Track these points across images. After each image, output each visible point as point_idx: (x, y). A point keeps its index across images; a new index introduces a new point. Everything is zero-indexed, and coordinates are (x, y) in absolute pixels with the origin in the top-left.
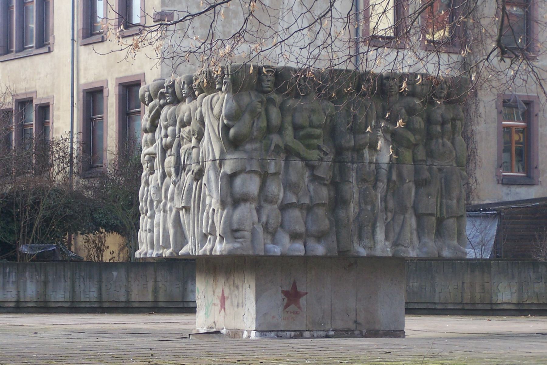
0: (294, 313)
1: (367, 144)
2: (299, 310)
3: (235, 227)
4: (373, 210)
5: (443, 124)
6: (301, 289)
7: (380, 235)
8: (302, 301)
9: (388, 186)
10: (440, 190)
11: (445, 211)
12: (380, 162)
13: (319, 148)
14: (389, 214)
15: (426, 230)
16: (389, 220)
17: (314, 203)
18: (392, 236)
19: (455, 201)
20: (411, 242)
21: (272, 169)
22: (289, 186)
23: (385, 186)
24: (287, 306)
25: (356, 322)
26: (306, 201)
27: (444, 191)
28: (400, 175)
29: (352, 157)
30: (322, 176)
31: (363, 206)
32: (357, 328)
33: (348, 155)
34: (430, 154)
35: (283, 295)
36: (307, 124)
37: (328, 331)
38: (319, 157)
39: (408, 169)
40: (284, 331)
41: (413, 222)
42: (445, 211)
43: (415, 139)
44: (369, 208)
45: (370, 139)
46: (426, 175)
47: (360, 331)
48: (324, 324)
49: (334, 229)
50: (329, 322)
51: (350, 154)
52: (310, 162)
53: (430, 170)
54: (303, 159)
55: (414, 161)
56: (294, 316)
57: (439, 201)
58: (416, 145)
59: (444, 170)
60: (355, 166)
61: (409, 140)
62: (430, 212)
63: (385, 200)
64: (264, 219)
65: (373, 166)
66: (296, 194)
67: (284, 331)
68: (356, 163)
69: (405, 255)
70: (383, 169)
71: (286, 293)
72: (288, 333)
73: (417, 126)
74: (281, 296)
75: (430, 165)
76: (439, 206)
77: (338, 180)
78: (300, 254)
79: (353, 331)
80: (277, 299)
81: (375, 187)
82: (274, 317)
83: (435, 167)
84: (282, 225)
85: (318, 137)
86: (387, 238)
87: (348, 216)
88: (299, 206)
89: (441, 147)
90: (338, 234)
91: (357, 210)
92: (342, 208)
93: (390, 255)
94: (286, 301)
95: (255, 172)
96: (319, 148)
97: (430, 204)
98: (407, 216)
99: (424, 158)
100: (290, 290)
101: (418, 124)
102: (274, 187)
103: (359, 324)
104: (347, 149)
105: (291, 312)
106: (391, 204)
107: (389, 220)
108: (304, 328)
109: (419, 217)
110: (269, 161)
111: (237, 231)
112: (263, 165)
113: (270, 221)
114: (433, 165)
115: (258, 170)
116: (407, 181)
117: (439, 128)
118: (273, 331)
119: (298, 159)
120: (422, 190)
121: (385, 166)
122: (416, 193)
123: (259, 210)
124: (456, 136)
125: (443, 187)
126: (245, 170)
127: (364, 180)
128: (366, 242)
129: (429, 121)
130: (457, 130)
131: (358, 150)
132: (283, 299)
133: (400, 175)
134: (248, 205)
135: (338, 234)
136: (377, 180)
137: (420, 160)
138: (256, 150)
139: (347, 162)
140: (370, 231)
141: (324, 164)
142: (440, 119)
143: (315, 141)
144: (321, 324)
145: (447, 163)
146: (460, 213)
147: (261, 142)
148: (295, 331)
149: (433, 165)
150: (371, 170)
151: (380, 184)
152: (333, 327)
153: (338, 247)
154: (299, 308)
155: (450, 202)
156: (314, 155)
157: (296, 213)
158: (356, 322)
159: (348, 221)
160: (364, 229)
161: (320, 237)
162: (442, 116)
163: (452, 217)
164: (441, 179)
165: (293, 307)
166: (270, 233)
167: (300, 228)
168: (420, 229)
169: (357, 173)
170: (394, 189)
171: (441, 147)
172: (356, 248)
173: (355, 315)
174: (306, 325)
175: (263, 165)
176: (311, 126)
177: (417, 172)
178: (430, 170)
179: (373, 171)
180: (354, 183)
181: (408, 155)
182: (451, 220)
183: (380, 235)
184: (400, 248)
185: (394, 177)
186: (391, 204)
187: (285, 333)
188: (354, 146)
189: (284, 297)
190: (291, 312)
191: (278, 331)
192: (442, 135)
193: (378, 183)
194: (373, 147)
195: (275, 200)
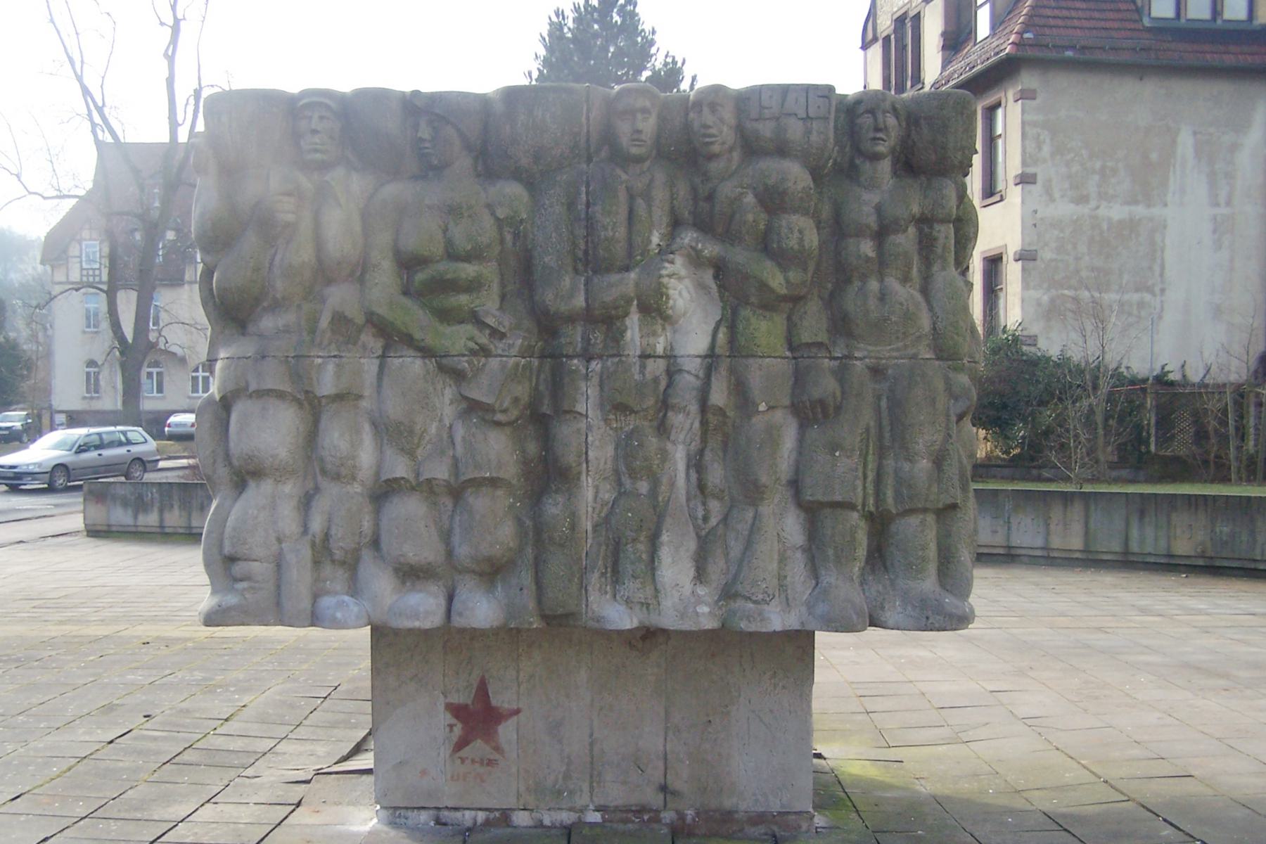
0: (482, 763)
1: (629, 302)
2: (497, 756)
3: (227, 550)
4: (654, 492)
5: (881, 234)
6: (501, 699)
7: (675, 569)
8: (506, 732)
9: (704, 423)
10: (873, 431)
11: (890, 493)
12: (676, 353)
13: (475, 319)
14: (714, 505)
15: (831, 552)
16: (713, 521)
17: (463, 478)
18: (717, 569)
19: (924, 464)
20: (782, 587)
21: (327, 384)
22: (392, 433)
23: (697, 425)
24: (461, 745)
25: (664, 788)
26: (440, 471)
27: (887, 435)
28: (740, 389)
29: (586, 340)
30: (484, 399)
31: (627, 482)
32: (669, 805)
33: (574, 336)
34: (841, 326)
35: (449, 716)
36: (438, 249)
37: (582, 810)
38: (471, 344)
39: (768, 369)
40: (456, 809)
41: (793, 527)
42: (890, 493)
43: (788, 281)
44: (644, 487)
45: (637, 285)
46: (826, 386)
47: (677, 812)
48: (571, 793)
49: (529, 550)
50: (586, 787)
51: (579, 329)
52: (444, 361)
53: (841, 374)
54: (426, 352)
55: (791, 348)
56: (481, 770)
57: (871, 466)
58: (796, 300)
59: (890, 371)
60: (596, 366)
61: (763, 286)
62: (838, 498)
63: (697, 464)
64: (317, 525)
65: (656, 367)
66: (411, 454)
67: (456, 809)
68: (600, 357)
69: (753, 628)
70: (689, 372)
71: (457, 711)
72: (467, 813)
73: (793, 243)
74: (445, 718)
75: (845, 357)
76: (871, 476)
77: (546, 408)
78: (417, 624)
79: (657, 811)
80: (439, 726)
81: (663, 429)
82: (424, 773)
83: (858, 363)
84: (376, 543)
85: (473, 286)
86: (701, 575)
87: (573, 515)
88: (427, 488)
89: (872, 303)
90: (538, 566)
91: (608, 495)
92: (556, 492)
93: (709, 624)
94: (458, 730)
95: (280, 395)
96: (475, 319)
97: (845, 474)
98: (766, 509)
99: (823, 337)
100: (469, 702)
101: (796, 234)
102: (336, 435)
103: (675, 793)
104: (571, 319)
105: (473, 761)
106: (716, 475)
107: (713, 521)
108: (510, 802)
109: (812, 512)
110: (320, 360)
111: (232, 559)
112: (298, 369)
113: (333, 532)
114: (849, 357)
115: (286, 387)
116: (762, 407)
117: (867, 248)
118: (424, 808)
119: (411, 352)
120: (814, 433)
121: (692, 366)
122: (801, 440)
123: (306, 503)
124: (935, 268)
125: (885, 422)
126: (246, 388)
127: (622, 408)
128: (630, 587)
129: (838, 229)
130: (939, 251)
131: (607, 320)
132: (451, 726)
133: (740, 389)
134: (267, 486)
135: (538, 566)
136: (665, 405)
137: (809, 345)
138: (287, 330)
139: (568, 356)
140: (644, 556)
141: (494, 363)
142: (872, 221)
143: (463, 299)
144: (560, 793)
145: (898, 350)
146: (946, 500)
148: (486, 809)
149: (849, 357)
150: (649, 376)
151: (676, 419)
152: (599, 801)
153: (539, 601)
154: (497, 749)
155: (907, 466)
156: (458, 338)
157: (409, 508)
158: (664, 788)
159: (573, 527)
160: (624, 550)
161: (492, 572)
162: (879, 209)
163: (912, 511)
164: (879, 398)
165: (478, 747)
166: (343, 563)
167: (425, 550)
168: (816, 548)
169: (601, 385)
170: (723, 432)
171: (872, 303)
172: (595, 607)
173: (662, 768)
174: (519, 796)
175: (298, 369)
176: (453, 255)
177: (800, 379)
178: (841, 374)
179: (656, 380)
180: (594, 415)
181: (766, 331)
182: (914, 521)
183: (675, 569)
184: (739, 604)
185: (719, 396)
186: (716, 475)
187: (458, 814)
188: (588, 308)
189: (454, 721)
190: (473, 761)
191: (438, 809)
192: (882, 264)
193: (670, 414)
194: (654, 308)
195: (344, 471)
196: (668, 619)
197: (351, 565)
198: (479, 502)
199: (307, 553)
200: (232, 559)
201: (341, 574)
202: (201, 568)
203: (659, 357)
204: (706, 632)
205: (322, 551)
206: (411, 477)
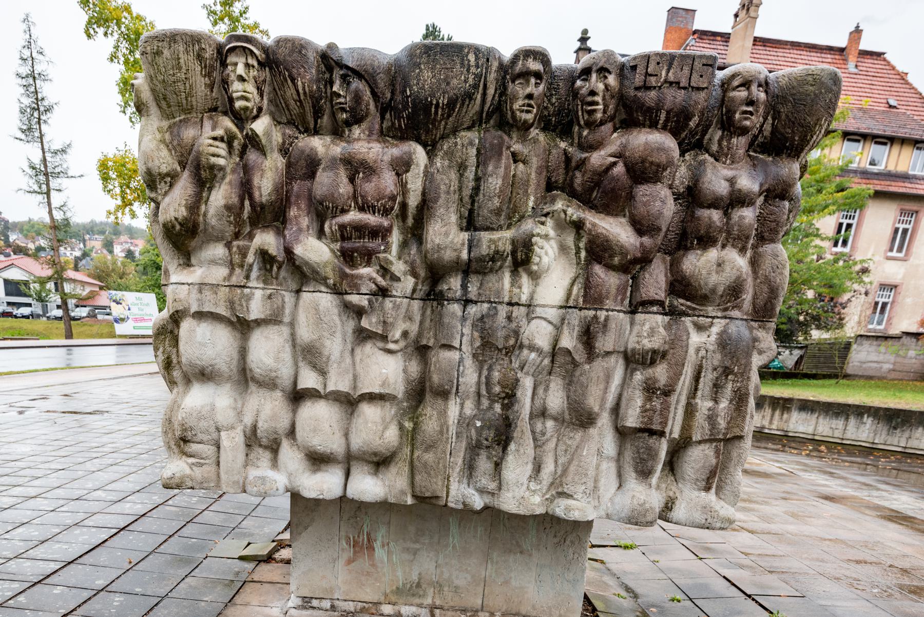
60: (473, 310)
84: (292, 432)
93: (540, 511)
115: (222, 310)
147: (228, 245)
161: (380, 462)
167: (333, 443)
183: (516, 467)
196: (509, 502)
197: (274, 448)
198: (370, 413)
199: (240, 439)
200: (185, 440)
201: (266, 455)
202: (334, 389)
203: (523, 305)
204: (535, 517)
205: (252, 439)
206: (319, 387)
